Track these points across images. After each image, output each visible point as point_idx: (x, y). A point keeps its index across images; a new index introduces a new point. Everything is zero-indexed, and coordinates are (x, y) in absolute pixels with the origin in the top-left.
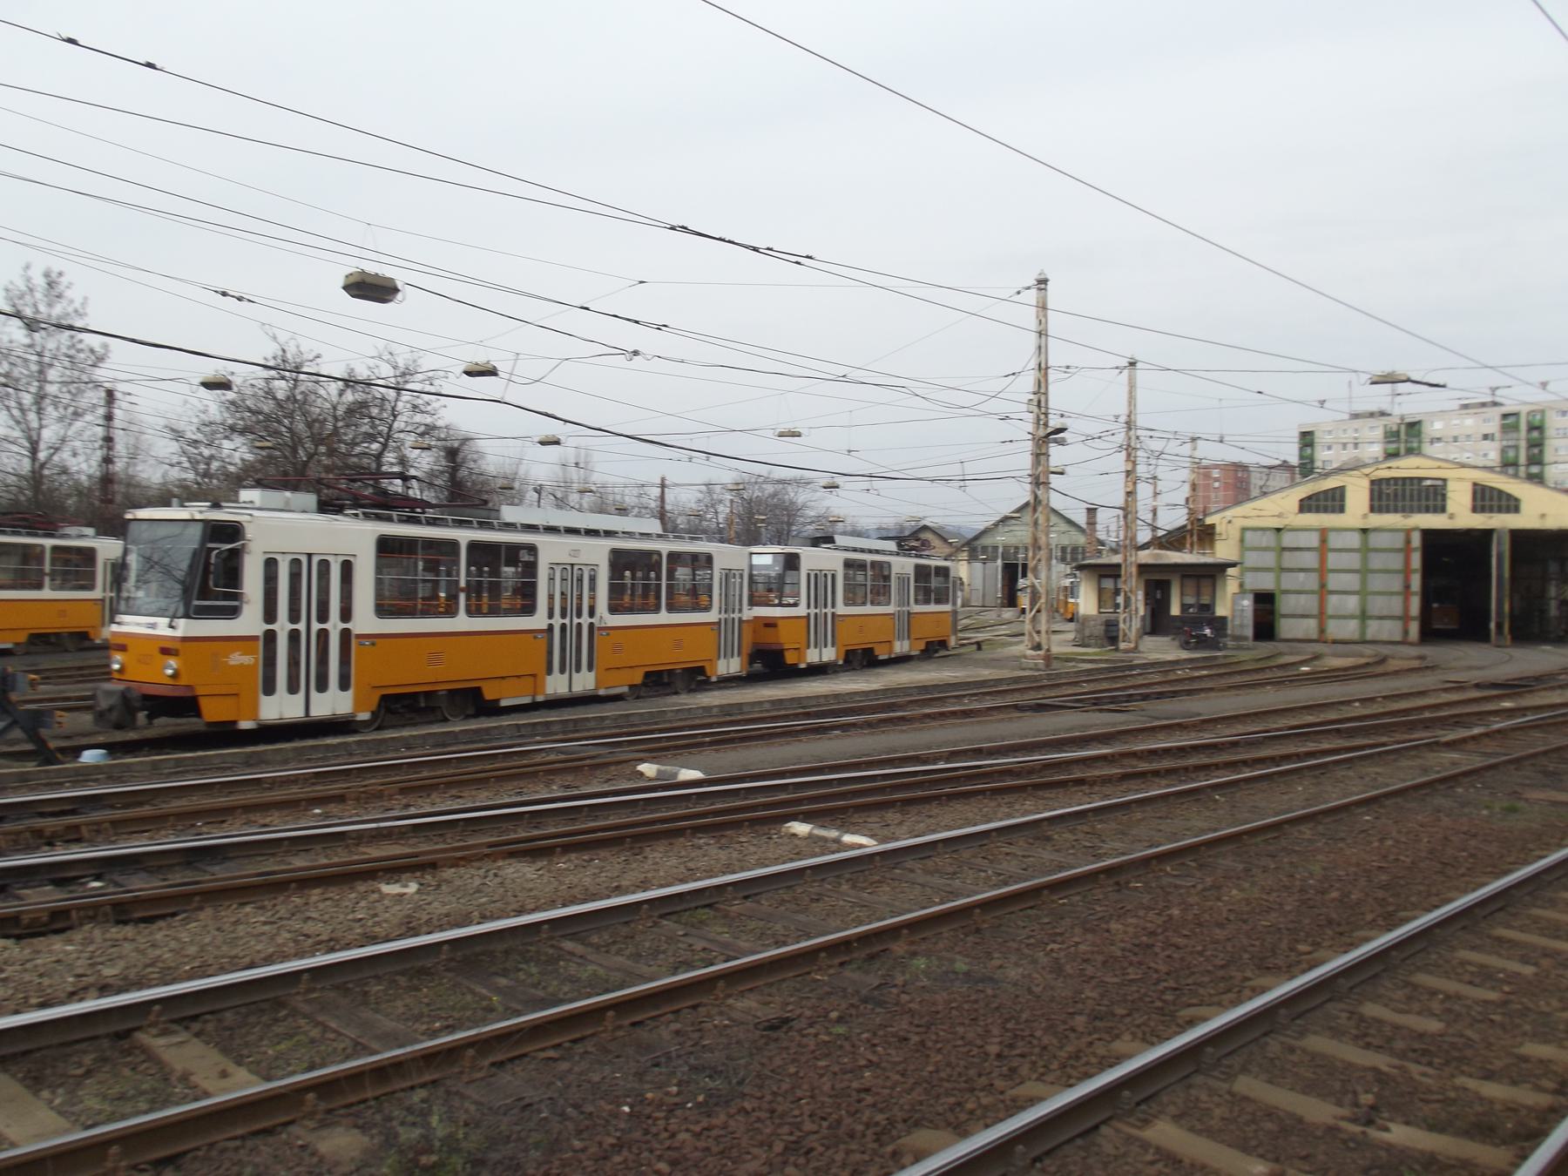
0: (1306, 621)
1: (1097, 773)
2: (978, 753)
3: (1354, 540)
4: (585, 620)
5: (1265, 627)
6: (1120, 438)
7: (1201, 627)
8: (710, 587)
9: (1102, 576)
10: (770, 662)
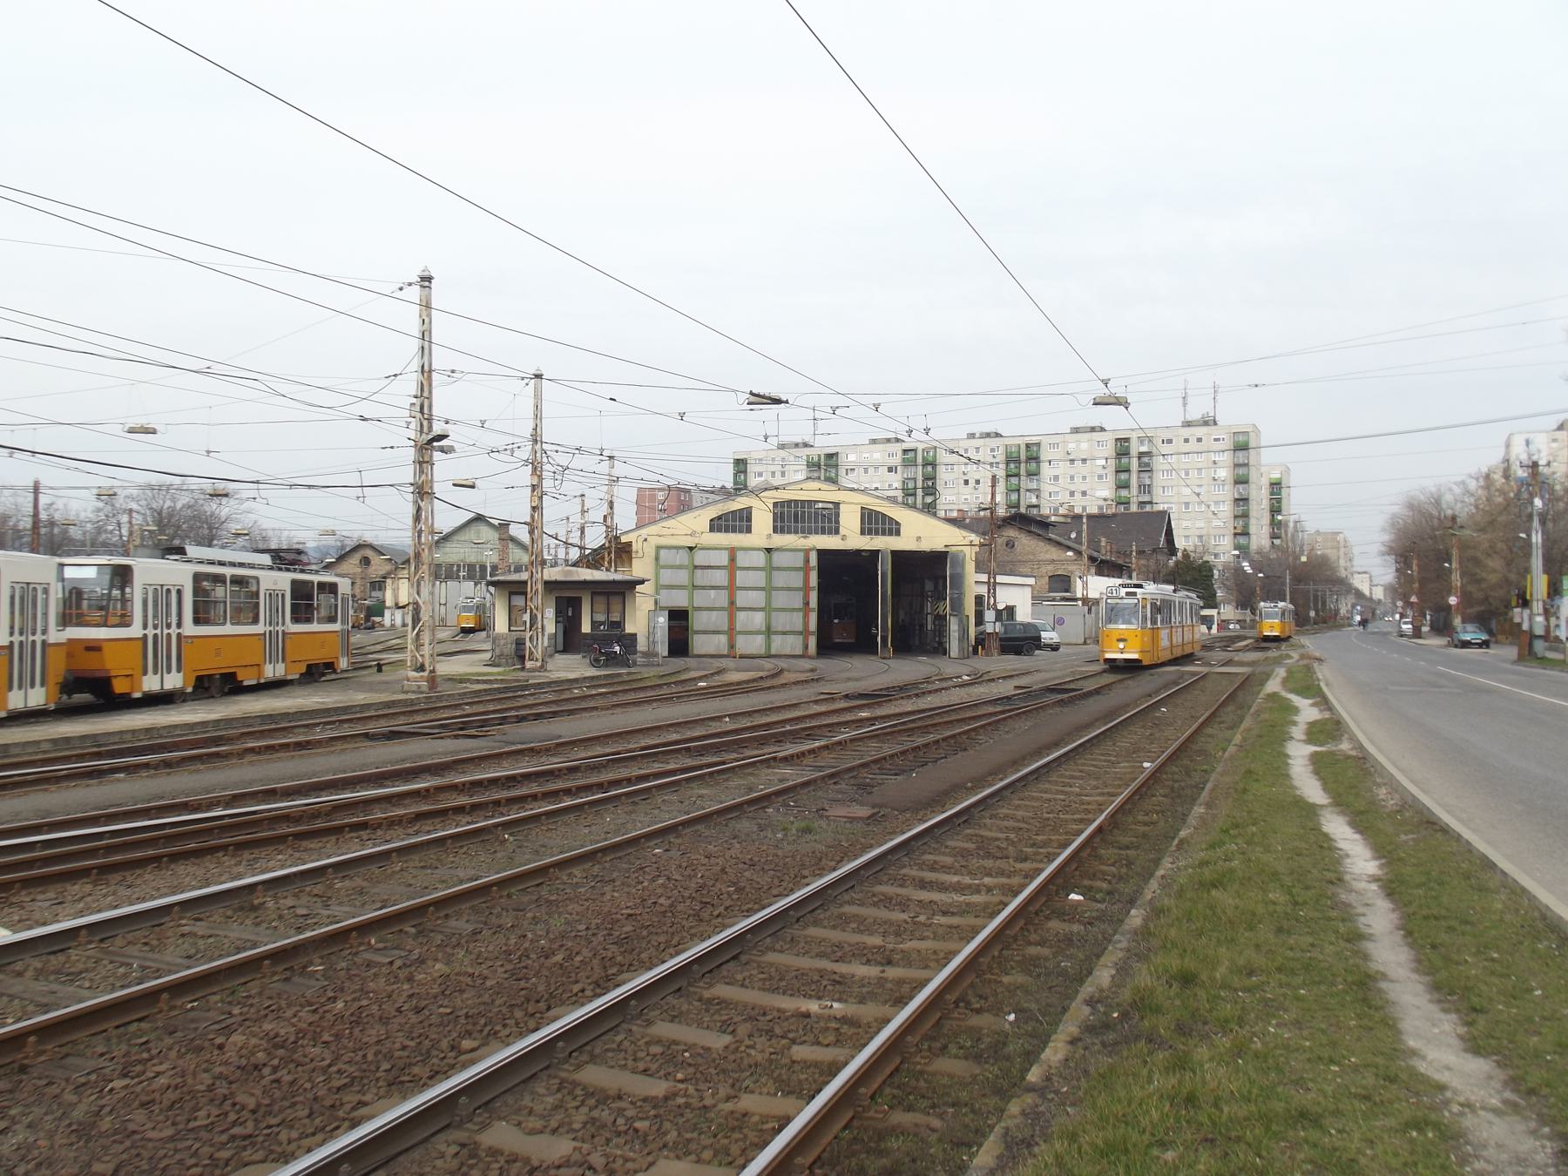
2: (271, 794)
3: (760, 559)
4: (38, 638)
5: (679, 644)
6: (525, 453)
7: (612, 645)
9: (511, 594)
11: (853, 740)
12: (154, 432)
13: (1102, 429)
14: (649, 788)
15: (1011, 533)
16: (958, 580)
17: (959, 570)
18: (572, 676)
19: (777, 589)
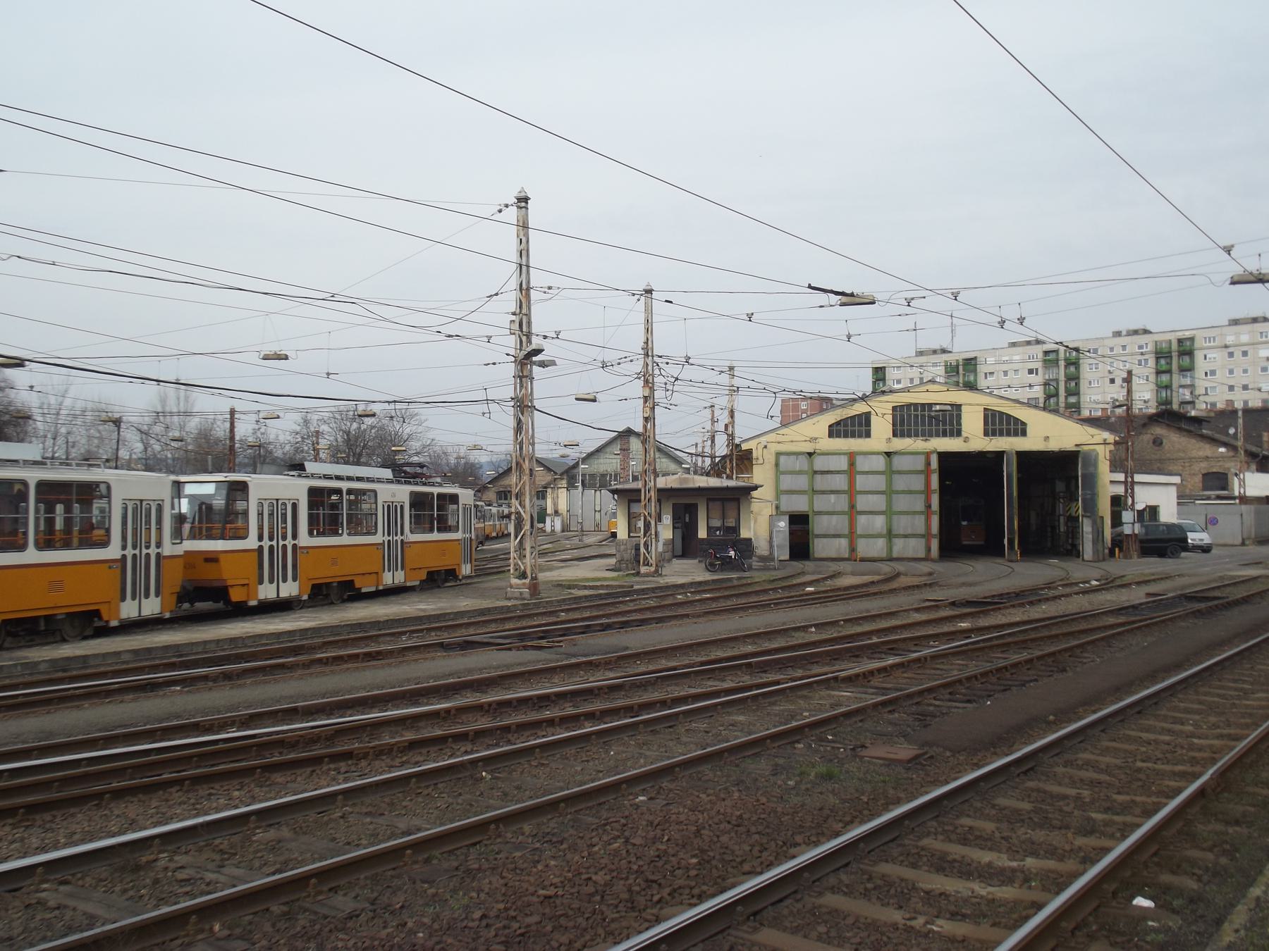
0: (837, 541)
2: (292, 714)
3: (879, 464)
5: (800, 546)
6: (638, 366)
7: (728, 550)
9: (630, 501)
10: (205, 596)
11: (934, 657)
12: (286, 358)
14: (677, 714)
15: (1159, 430)
16: (1091, 481)
17: (1091, 469)
18: (681, 581)
19: (898, 492)
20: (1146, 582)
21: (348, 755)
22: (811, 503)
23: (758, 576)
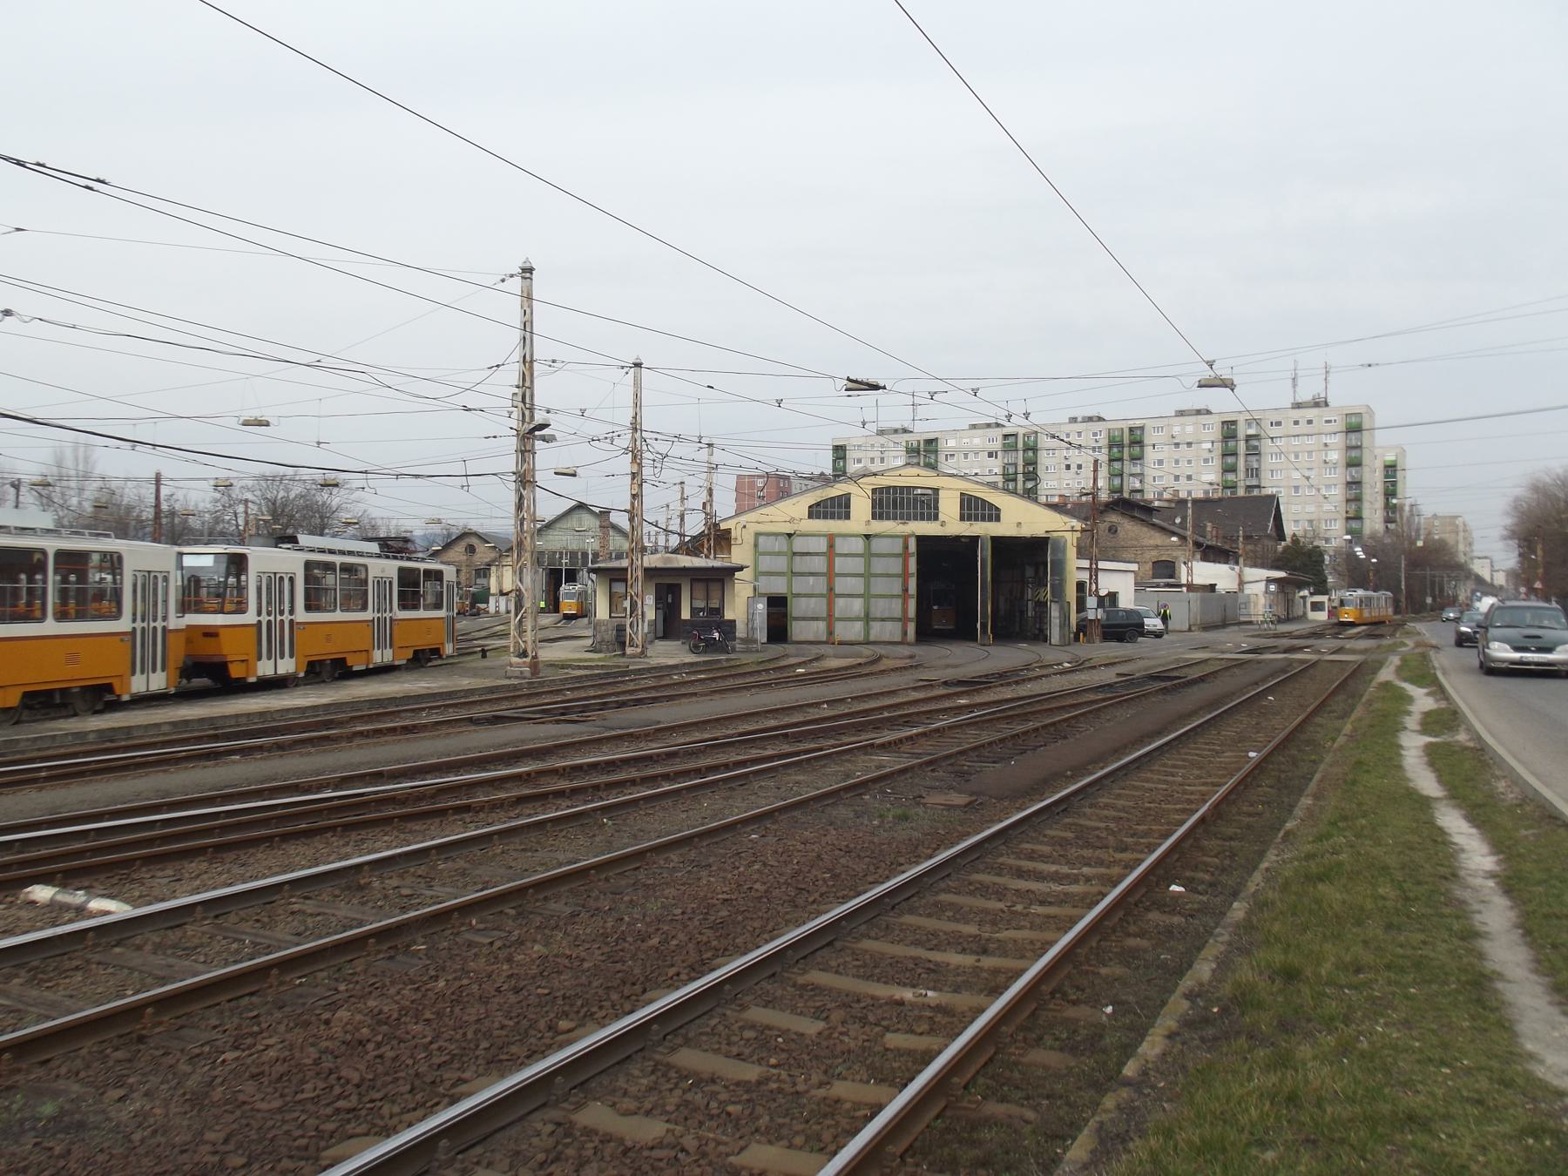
0: (815, 624)
1: (503, 795)
2: (378, 777)
3: (858, 546)
5: (778, 630)
6: (625, 441)
7: (711, 631)
8: (44, 590)
9: (612, 581)
10: (207, 673)
11: (950, 728)
12: (268, 424)
13: (1208, 412)
15: (1114, 518)
16: (1059, 566)
17: (1060, 556)
18: (671, 662)
20: (1113, 664)
21: (467, 808)
22: (790, 585)
23: (747, 658)
